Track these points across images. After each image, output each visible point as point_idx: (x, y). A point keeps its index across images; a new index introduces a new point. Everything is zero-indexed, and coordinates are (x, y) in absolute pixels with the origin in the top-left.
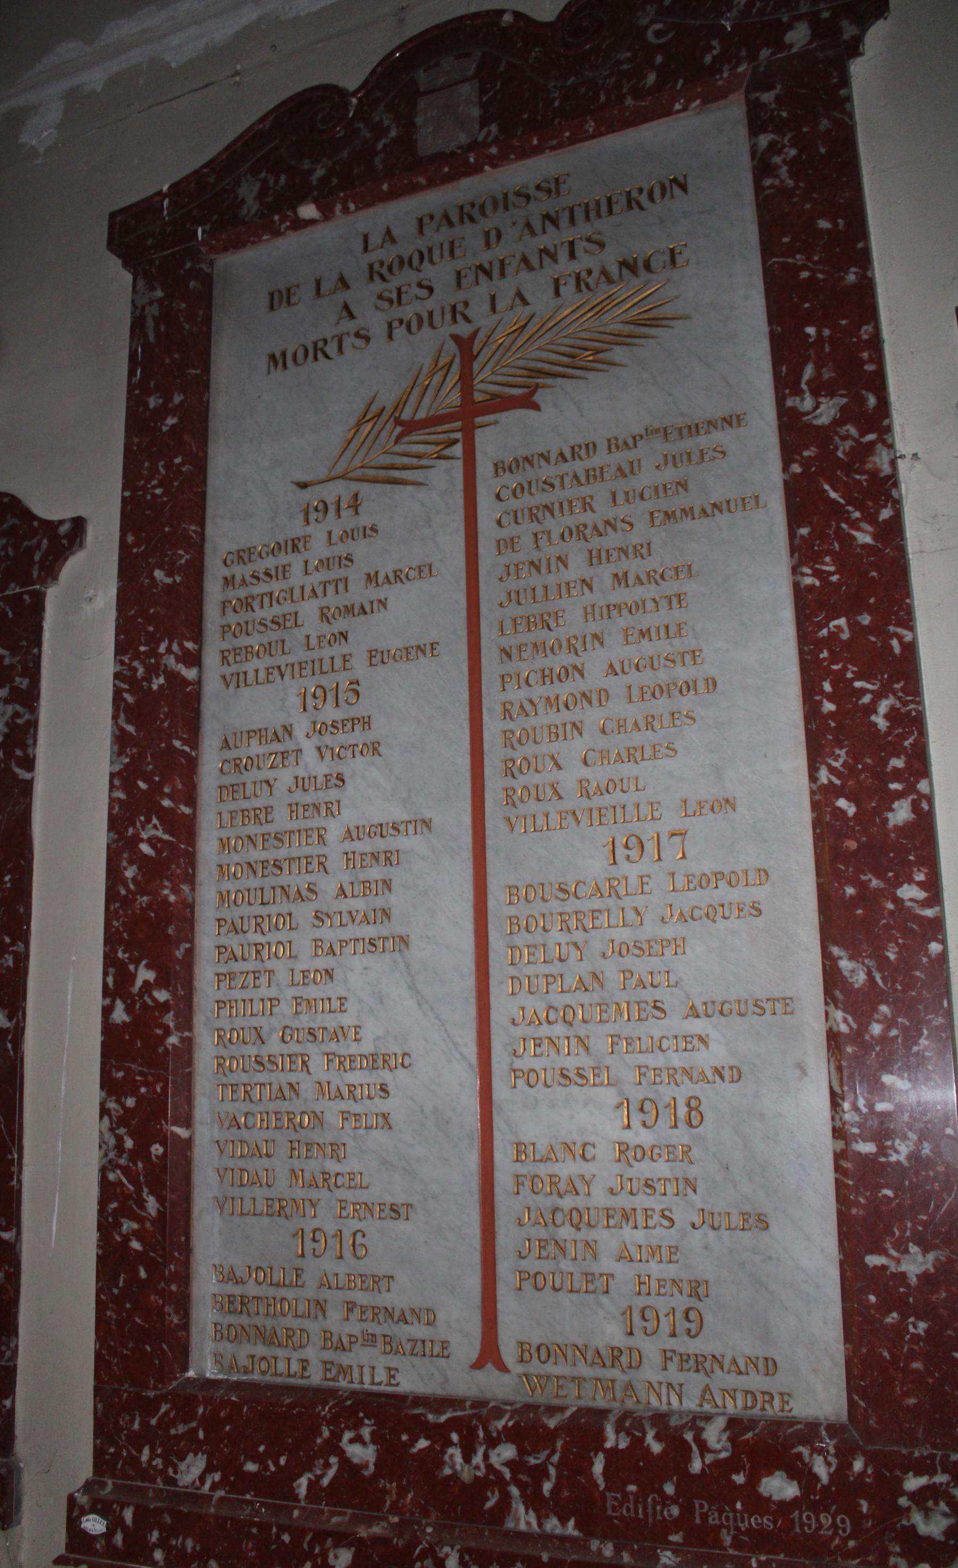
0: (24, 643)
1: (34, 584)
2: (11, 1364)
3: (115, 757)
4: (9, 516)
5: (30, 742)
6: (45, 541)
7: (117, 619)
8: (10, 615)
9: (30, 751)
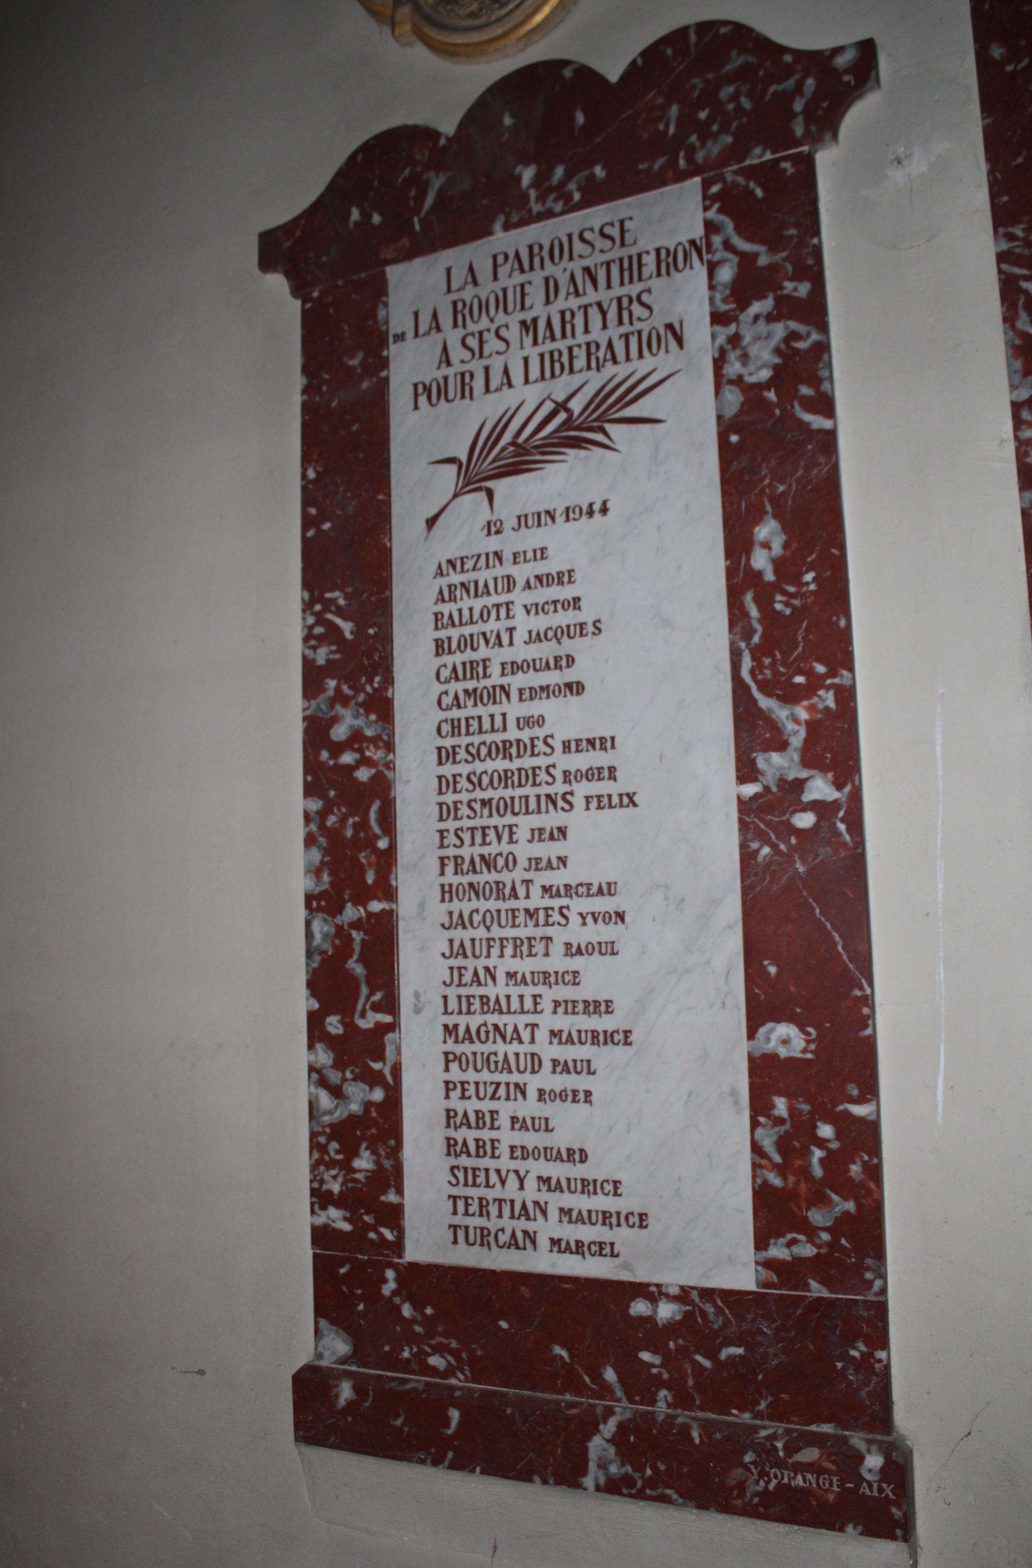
0: (792, 232)
1: (799, 144)
2: (881, 1298)
3: (1017, 379)
4: (734, 53)
5: (824, 373)
6: (810, 81)
7: (990, 173)
8: (759, 193)
9: (825, 386)
